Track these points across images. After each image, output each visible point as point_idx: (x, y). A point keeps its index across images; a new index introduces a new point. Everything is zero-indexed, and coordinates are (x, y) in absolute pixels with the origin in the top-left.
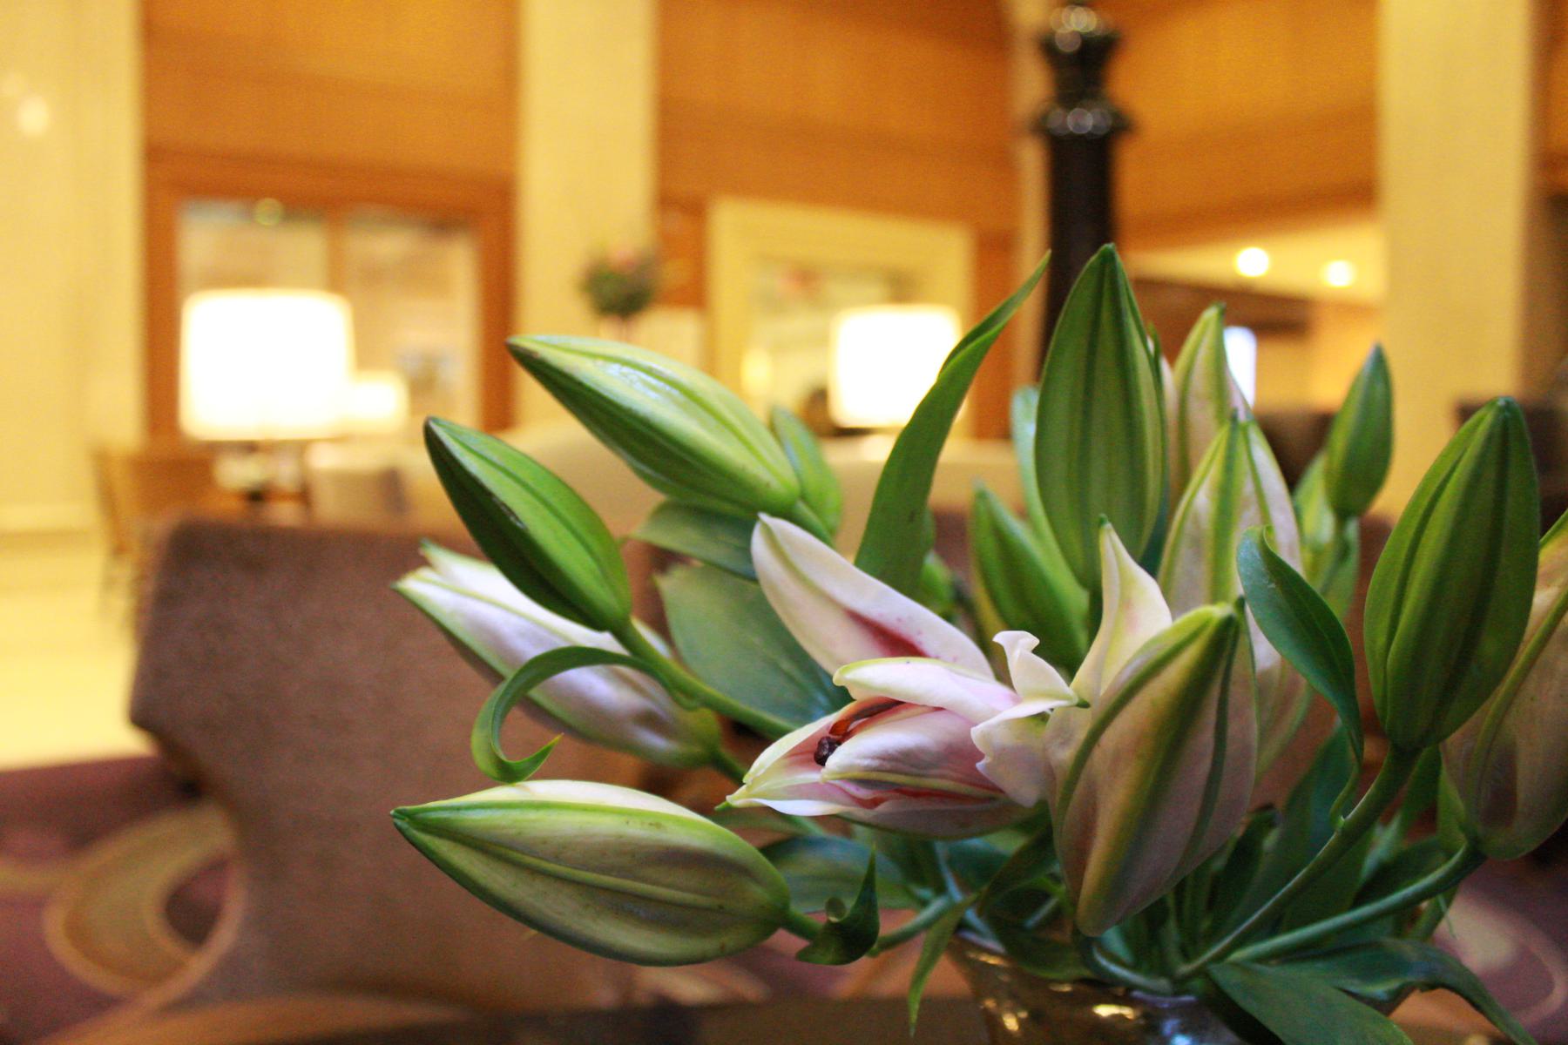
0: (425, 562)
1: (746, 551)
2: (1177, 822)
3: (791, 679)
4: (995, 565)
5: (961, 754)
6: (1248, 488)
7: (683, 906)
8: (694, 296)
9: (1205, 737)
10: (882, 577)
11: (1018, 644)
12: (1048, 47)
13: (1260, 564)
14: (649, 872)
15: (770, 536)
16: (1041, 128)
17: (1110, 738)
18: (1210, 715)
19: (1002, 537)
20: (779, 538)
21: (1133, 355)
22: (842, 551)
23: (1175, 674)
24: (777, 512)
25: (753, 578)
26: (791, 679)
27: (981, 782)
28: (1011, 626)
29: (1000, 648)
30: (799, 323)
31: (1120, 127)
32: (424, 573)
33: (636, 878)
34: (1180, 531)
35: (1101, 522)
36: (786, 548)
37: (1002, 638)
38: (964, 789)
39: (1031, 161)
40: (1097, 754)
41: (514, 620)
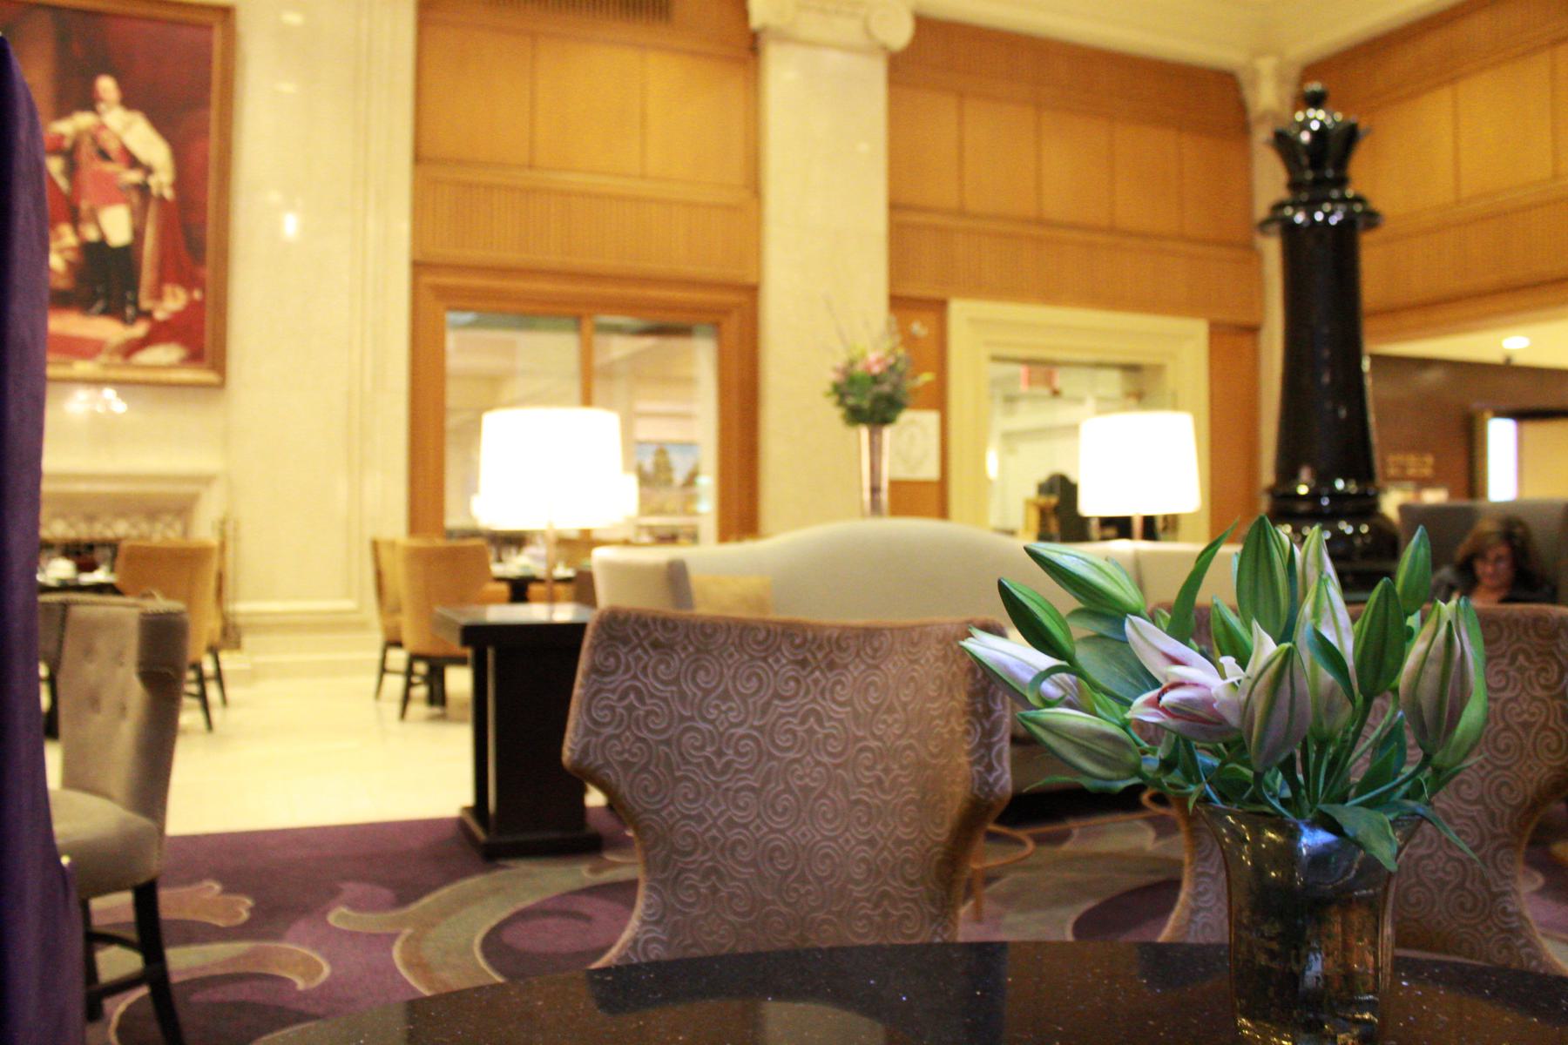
0: (971, 635)
1: (1123, 633)
2: (1281, 714)
3: (1133, 685)
4: (1223, 640)
5: (1207, 703)
6: (1325, 603)
7: (1103, 755)
8: (937, 399)
9: (1286, 686)
10: (1176, 638)
11: (1228, 661)
12: (1284, 142)
13: (1312, 633)
14: (1097, 741)
15: (1132, 623)
16: (1277, 216)
17: (1257, 687)
18: (1287, 677)
19: (1224, 623)
20: (1137, 625)
21: (1273, 554)
22: (1369, 597)
23: (1275, 665)
24: (1137, 614)
25: (1126, 642)
26: (1133, 685)
27: (1214, 712)
28: (1223, 654)
29: (1222, 665)
30: (1028, 416)
31: (1363, 218)
32: (970, 639)
33: (1093, 743)
34: (111, 605)
35: (1252, 618)
36: (1139, 629)
37: (1223, 660)
38: (1209, 718)
39: (1271, 249)
40: (1254, 693)
41: (1014, 660)
